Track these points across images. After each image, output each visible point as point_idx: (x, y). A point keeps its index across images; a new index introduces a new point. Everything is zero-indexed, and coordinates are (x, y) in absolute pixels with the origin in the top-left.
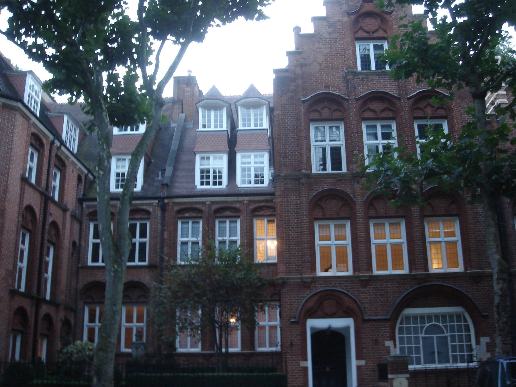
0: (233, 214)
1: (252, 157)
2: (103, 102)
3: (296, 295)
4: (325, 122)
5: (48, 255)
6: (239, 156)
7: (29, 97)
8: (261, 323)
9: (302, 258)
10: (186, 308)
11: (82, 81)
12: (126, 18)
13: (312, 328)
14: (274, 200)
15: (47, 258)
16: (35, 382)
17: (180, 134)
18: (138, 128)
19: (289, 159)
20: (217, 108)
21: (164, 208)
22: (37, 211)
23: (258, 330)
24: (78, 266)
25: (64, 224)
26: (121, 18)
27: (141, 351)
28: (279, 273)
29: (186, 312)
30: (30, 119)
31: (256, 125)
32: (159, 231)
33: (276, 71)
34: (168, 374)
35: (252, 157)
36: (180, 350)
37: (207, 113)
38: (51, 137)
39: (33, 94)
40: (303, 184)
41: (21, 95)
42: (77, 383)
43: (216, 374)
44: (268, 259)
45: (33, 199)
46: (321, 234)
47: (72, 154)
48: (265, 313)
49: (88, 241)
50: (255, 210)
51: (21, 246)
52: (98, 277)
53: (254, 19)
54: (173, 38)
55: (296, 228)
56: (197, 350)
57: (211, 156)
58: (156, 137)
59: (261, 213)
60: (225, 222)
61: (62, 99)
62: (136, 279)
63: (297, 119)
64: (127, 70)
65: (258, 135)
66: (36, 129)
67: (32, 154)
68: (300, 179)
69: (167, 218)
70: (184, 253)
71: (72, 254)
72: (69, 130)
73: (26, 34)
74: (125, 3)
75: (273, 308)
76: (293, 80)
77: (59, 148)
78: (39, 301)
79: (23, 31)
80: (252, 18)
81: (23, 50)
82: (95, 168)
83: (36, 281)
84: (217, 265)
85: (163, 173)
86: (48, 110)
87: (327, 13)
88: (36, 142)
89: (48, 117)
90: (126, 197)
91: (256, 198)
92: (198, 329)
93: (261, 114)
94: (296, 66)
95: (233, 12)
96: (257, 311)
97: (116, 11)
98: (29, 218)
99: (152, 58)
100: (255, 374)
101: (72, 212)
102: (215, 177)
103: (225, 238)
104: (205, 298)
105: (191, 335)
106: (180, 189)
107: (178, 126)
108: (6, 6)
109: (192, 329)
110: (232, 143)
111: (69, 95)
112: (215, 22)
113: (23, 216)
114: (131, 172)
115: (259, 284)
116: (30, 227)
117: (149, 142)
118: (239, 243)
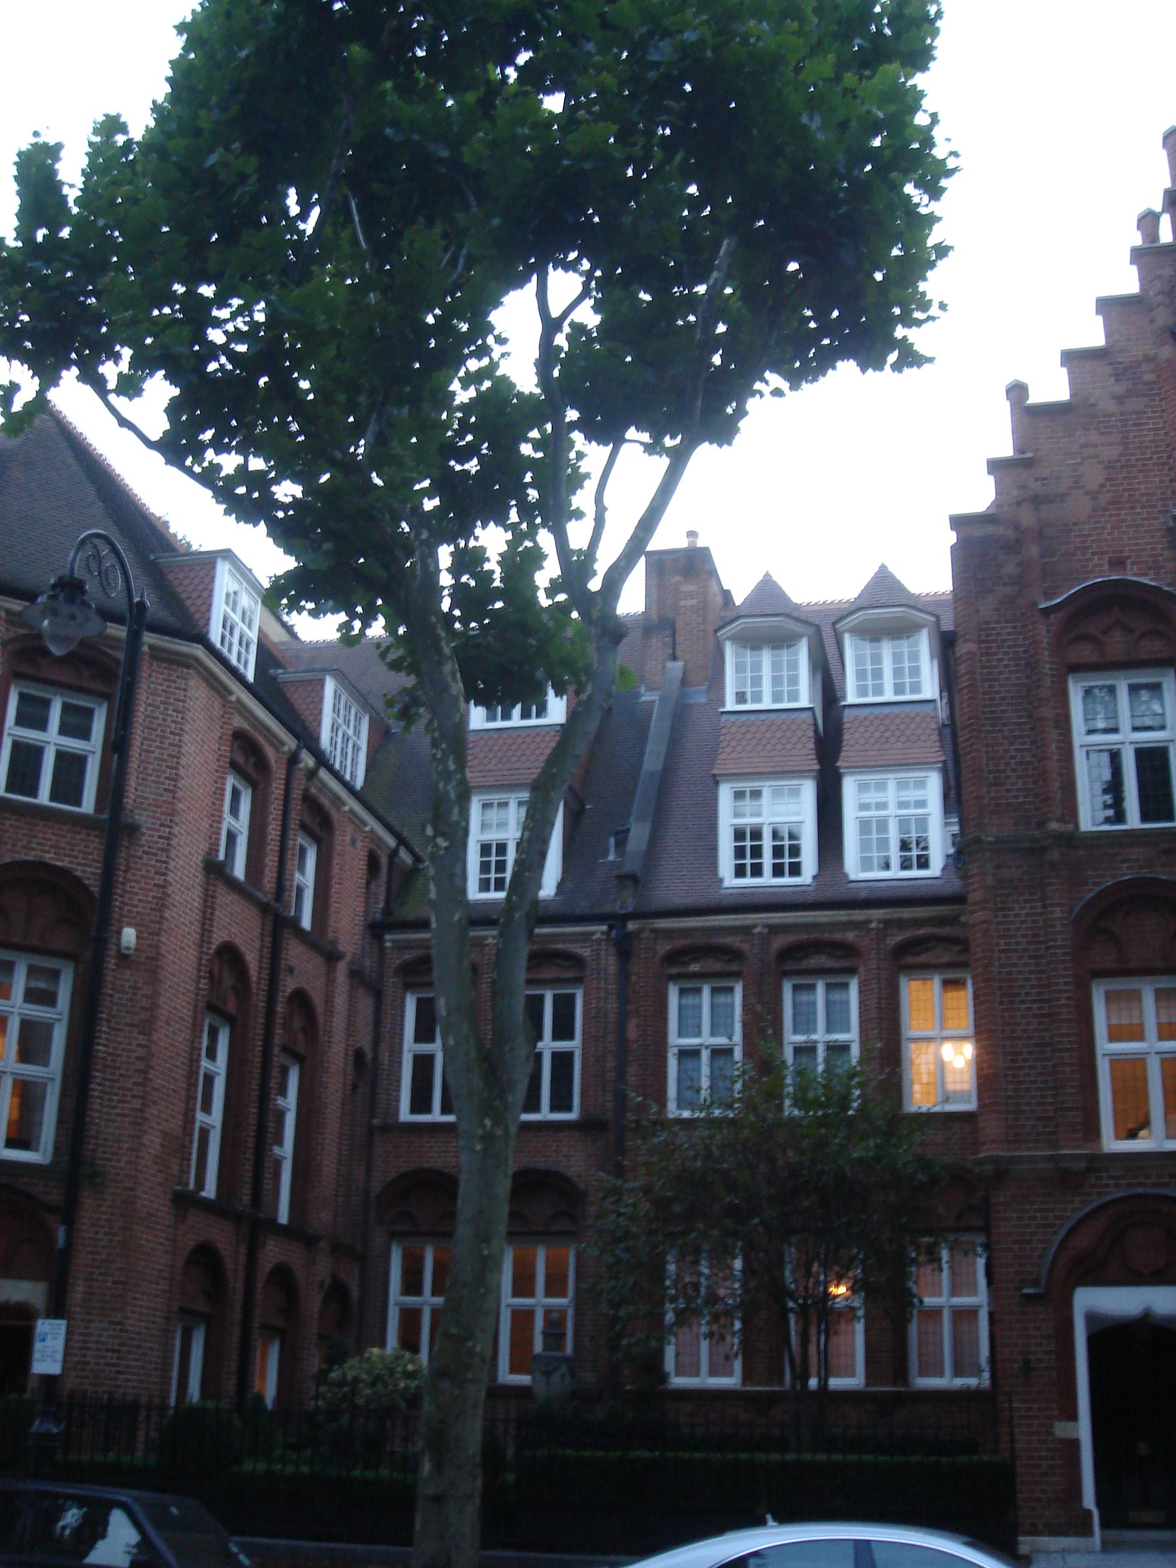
0: (836, 964)
1: (891, 785)
2: (443, 635)
3: (1038, 1210)
4: (1117, 673)
5: (283, 1091)
6: (850, 787)
7: (224, 627)
8: (929, 1301)
9: (1054, 1096)
10: (697, 1251)
11: (381, 573)
12: (503, 384)
13: (1091, 1318)
14: (963, 919)
15: (280, 1101)
16: (248, 1467)
17: (668, 724)
18: (542, 711)
19: (1007, 791)
20: (780, 641)
21: (624, 948)
22: (251, 958)
23: (919, 1323)
24: (372, 1125)
25: (329, 1000)
26: (487, 384)
27: (559, 1383)
28: (984, 1143)
29: (697, 1262)
30: (231, 693)
31: (899, 689)
32: (612, 1017)
33: (958, 522)
34: (647, 1454)
35: (891, 785)
36: (678, 1382)
37: (749, 657)
38: (290, 743)
39: (235, 618)
40: (1053, 865)
41: (201, 623)
42: (370, 1474)
43: (790, 1456)
44: (947, 1100)
45: (239, 925)
46: (1114, 1022)
47: (349, 787)
48: (941, 1270)
49: (401, 1048)
50: (903, 949)
51: (205, 1063)
52: (434, 1157)
53: (887, 367)
54: (645, 437)
55: (1033, 1002)
56: (731, 1381)
57: (766, 787)
58: (599, 737)
59: (922, 958)
60: (812, 987)
61: (317, 628)
62: (541, 1163)
63: (1028, 664)
64: (509, 536)
65: (907, 720)
66: (246, 719)
67: (236, 794)
68: (1043, 849)
69: (634, 978)
70: (688, 1084)
71: (355, 1087)
72: (340, 721)
73: (220, 447)
74: (500, 340)
75: (966, 1254)
76: (1012, 547)
77: (312, 774)
78: (257, 1227)
79: (208, 435)
80: (879, 365)
81: (210, 493)
82: (423, 828)
83: (249, 1167)
84: (792, 1119)
85: (621, 844)
86: (279, 665)
87: (1107, 336)
88: (247, 757)
89: (281, 683)
90: (517, 916)
91: (907, 913)
92: (729, 1314)
93: (914, 656)
94: (1019, 504)
95: (821, 350)
96: (914, 1261)
97: (473, 365)
98: (229, 981)
99: (582, 499)
100: (915, 1459)
101: (352, 962)
102: (778, 852)
103: (814, 1037)
104: (756, 1221)
105: (711, 1335)
106: (672, 888)
107: (663, 699)
108: (160, 369)
109: (715, 1318)
110: (829, 746)
111: (342, 617)
112: (767, 383)
113: (211, 973)
114: (530, 840)
115: (921, 1177)
116: (231, 1007)
117: (581, 748)
118: (855, 1051)
